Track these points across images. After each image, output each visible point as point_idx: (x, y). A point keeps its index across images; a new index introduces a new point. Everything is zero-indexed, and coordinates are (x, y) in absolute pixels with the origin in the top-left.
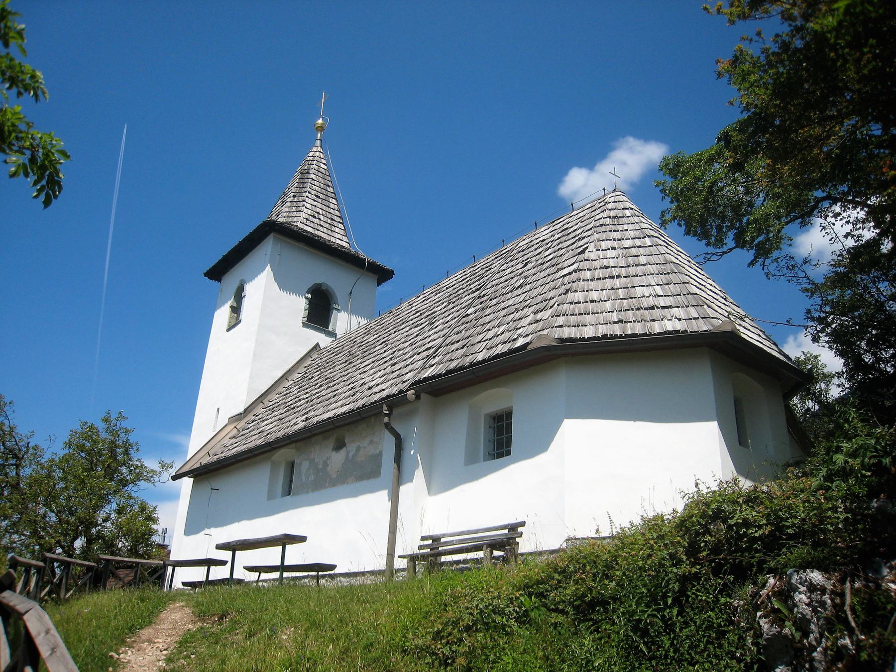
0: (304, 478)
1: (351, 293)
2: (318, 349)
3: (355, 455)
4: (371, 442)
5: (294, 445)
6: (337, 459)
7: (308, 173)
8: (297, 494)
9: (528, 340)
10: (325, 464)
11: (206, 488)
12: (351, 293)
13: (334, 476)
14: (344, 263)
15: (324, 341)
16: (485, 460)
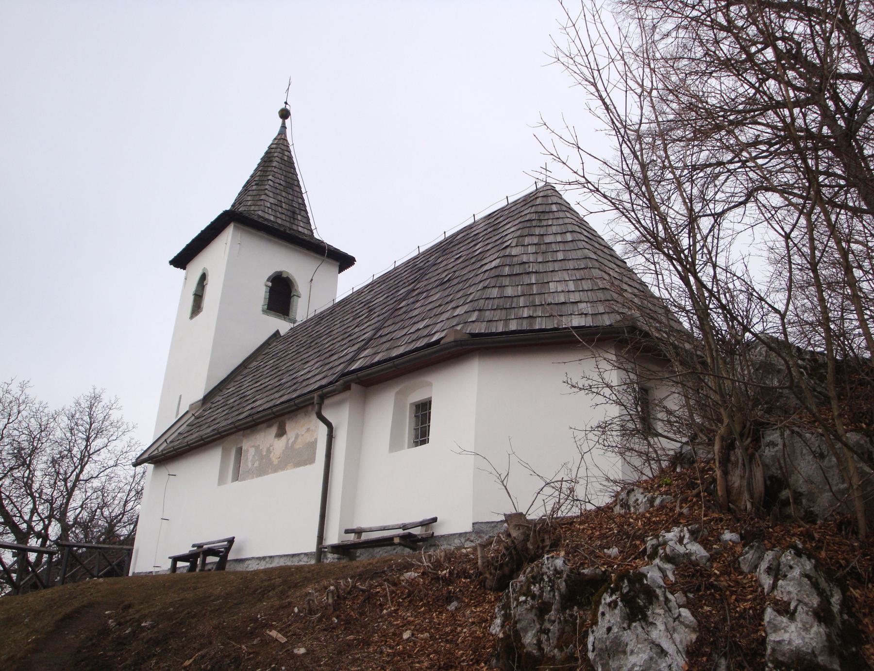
0: (250, 465)
1: (312, 280)
2: (278, 336)
3: (294, 442)
4: (308, 430)
5: (241, 433)
6: (280, 445)
7: (271, 161)
8: (244, 479)
9: (443, 335)
10: (269, 451)
11: (165, 471)
12: (312, 280)
13: (276, 462)
14: (307, 252)
15: (283, 326)
16: (409, 448)
